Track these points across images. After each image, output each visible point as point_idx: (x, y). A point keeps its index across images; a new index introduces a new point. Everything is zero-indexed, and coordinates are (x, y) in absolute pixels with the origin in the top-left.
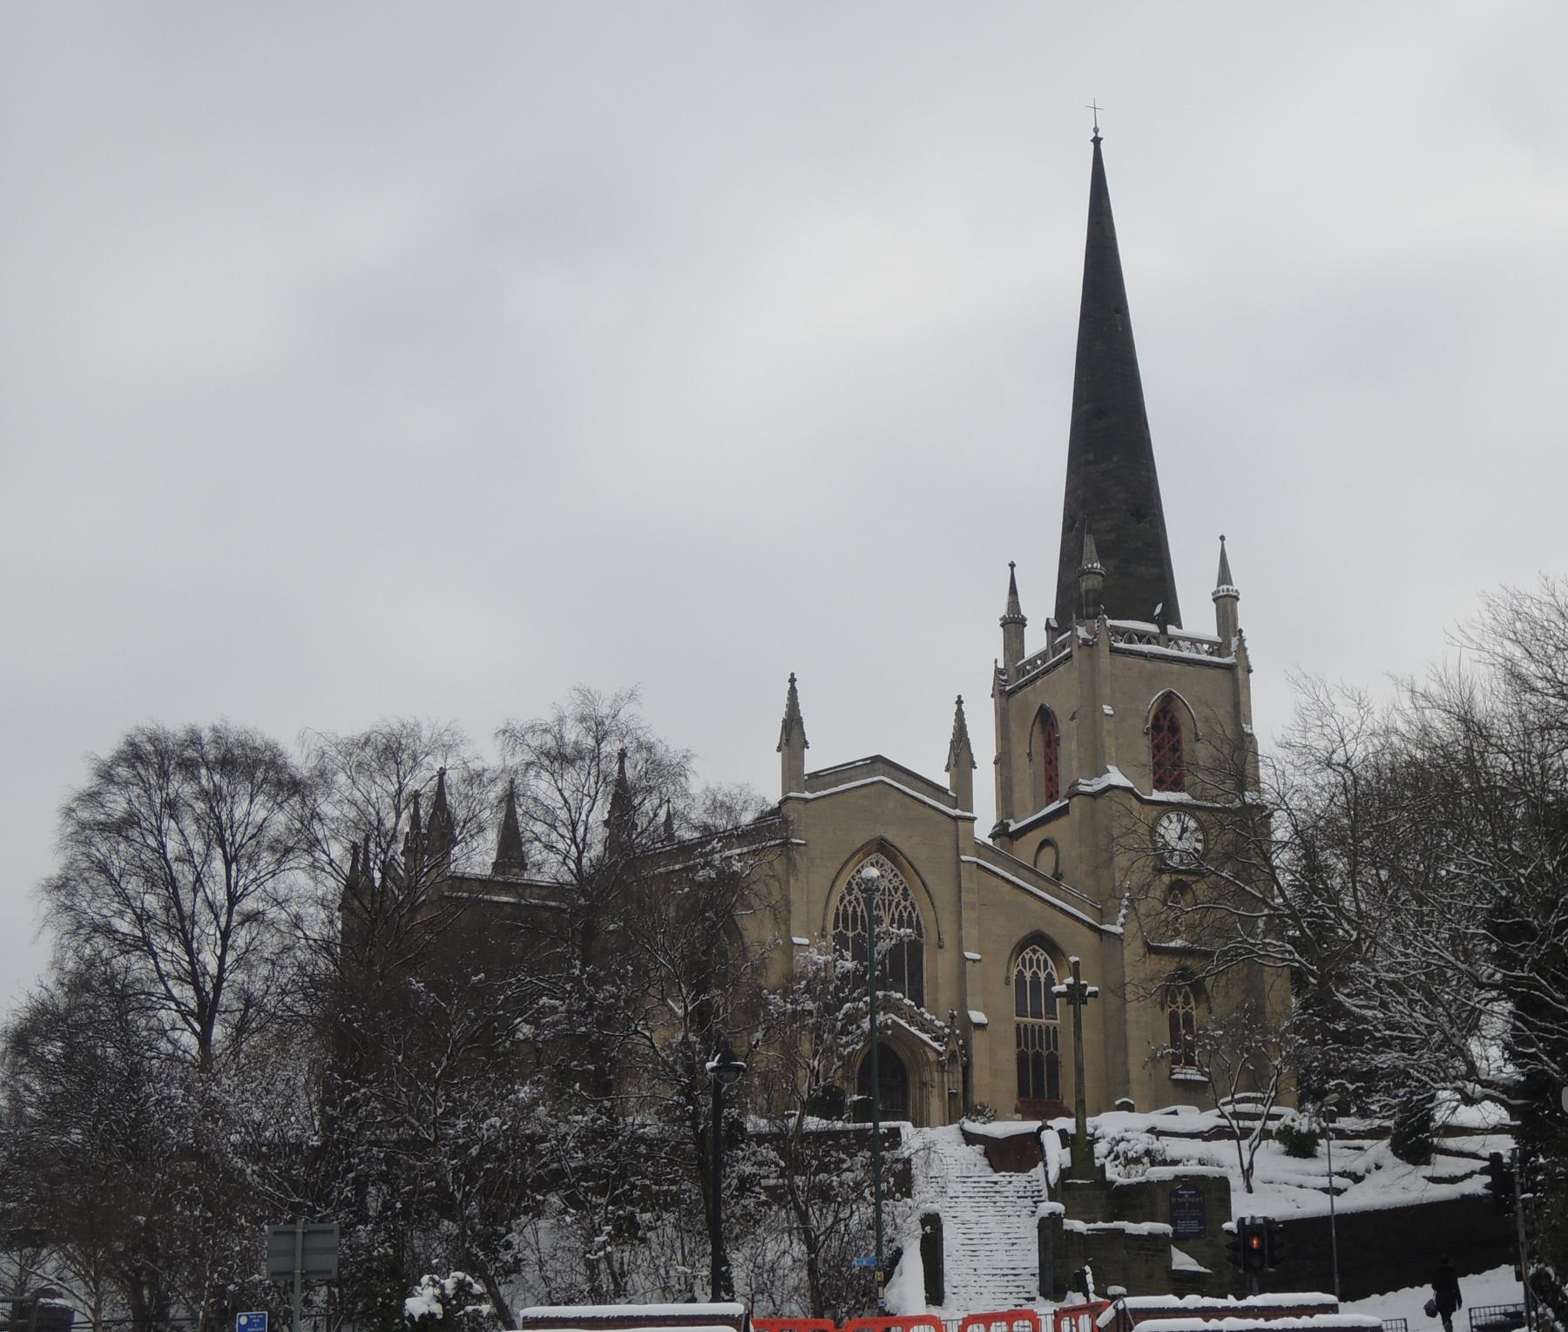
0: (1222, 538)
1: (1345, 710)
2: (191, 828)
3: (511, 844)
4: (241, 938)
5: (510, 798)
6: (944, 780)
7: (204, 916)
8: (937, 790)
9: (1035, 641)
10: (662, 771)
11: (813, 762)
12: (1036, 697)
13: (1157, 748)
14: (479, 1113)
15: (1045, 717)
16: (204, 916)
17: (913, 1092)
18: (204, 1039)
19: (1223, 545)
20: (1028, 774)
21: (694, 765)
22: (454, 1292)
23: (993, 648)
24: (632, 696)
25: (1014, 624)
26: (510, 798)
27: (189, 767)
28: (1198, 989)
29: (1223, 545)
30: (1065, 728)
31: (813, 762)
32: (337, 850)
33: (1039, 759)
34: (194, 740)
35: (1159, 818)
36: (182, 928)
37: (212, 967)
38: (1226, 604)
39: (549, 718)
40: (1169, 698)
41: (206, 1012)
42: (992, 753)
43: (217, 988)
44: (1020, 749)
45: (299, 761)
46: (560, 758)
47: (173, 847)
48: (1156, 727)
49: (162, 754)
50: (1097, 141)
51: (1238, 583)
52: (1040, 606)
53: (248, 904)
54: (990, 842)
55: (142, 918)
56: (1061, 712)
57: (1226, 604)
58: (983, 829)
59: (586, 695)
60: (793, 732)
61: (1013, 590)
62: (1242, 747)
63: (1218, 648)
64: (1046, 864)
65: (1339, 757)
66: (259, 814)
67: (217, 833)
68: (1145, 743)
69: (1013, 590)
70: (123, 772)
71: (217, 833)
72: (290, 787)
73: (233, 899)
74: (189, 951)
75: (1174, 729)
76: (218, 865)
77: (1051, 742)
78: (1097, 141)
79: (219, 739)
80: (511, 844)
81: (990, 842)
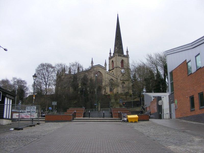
1: (135, 62)
2: (45, 70)
3: (70, 72)
4: (49, 79)
5: (70, 68)
6: (104, 66)
8: (104, 67)
9: (112, 55)
10: (81, 67)
11: (94, 65)
13: (122, 64)
14: (134, 76)
15: (113, 61)
18: (46, 87)
20: (111, 66)
22: (85, 70)
23: (109, 55)
25: (110, 53)
26: (70, 68)
27: (45, 66)
28: (124, 83)
30: (114, 62)
32: (56, 72)
33: (112, 64)
35: (121, 70)
36: (45, 78)
37: (47, 81)
38: (127, 52)
40: (123, 60)
41: (46, 84)
43: (47, 83)
45: (53, 65)
46: (73, 65)
47: (44, 72)
48: (121, 62)
49: (43, 65)
50: (118, 15)
52: (112, 52)
54: (108, 71)
57: (127, 52)
58: (108, 70)
60: (92, 62)
61: (110, 51)
62: (128, 63)
64: (112, 73)
65: (134, 66)
67: (47, 71)
68: (120, 64)
69: (110, 51)
71: (47, 71)
72: (52, 67)
74: (45, 80)
75: (123, 62)
77: (113, 63)
78: (118, 15)
80: (70, 72)
81: (108, 71)
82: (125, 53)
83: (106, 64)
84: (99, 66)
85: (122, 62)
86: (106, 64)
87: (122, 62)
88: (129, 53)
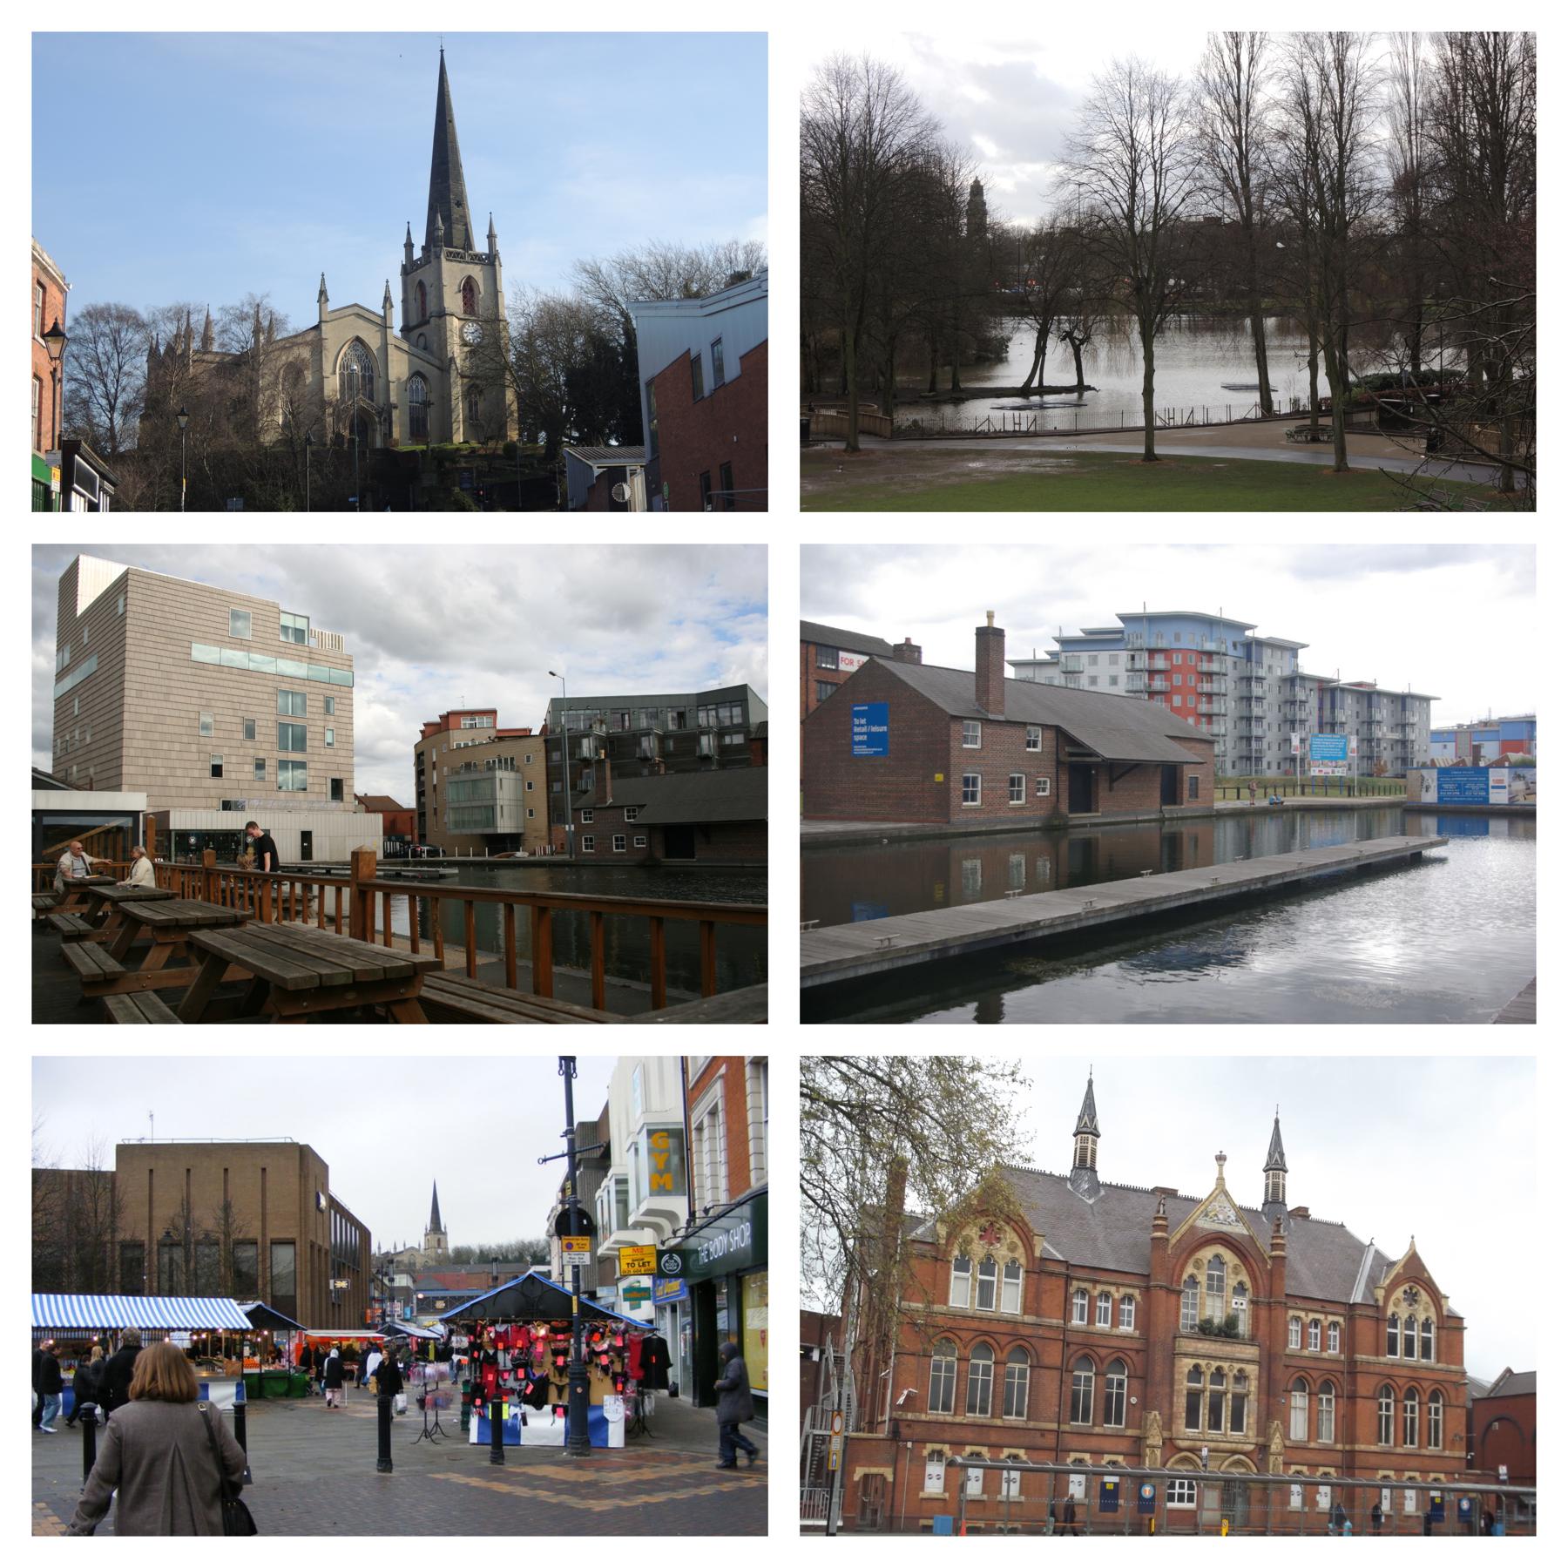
0: (1221, 1158)
7: (110, 372)
9: (417, 254)
12: (420, 275)
15: (421, 284)
16: (110, 372)
17: (370, 433)
19: (1221, 1172)
21: (289, 319)
23: (401, 257)
24: (267, 295)
25: (409, 246)
29: (1221, 1172)
31: (331, 306)
33: (419, 301)
34: (108, 308)
36: (102, 377)
37: (113, 391)
38: (491, 237)
39: (238, 304)
42: (400, 297)
43: (116, 399)
44: (411, 296)
45: (145, 316)
46: (242, 318)
47: (100, 349)
50: (442, 51)
51: (496, 231)
52: (419, 240)
53: (126, 368)
55: (89, 374)
56: (427, 283)
57: (491, 237)
59: (251, 295)
61: (409, 233)
63: (488, 256)
66: (130, 336)
69: (409, 233)
70: (82, 320)
73: (120, 368)
76: (116, 355)
77: (424, 295)
78: (442, 51)
79: (117, 308)
82: (480, 246)
83: (387, 299)
84: (412, 1248)
85: (439, 1240)
86: (387, 299)
87: (439, 1240)
88: (500, 246)
